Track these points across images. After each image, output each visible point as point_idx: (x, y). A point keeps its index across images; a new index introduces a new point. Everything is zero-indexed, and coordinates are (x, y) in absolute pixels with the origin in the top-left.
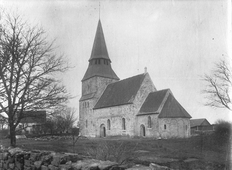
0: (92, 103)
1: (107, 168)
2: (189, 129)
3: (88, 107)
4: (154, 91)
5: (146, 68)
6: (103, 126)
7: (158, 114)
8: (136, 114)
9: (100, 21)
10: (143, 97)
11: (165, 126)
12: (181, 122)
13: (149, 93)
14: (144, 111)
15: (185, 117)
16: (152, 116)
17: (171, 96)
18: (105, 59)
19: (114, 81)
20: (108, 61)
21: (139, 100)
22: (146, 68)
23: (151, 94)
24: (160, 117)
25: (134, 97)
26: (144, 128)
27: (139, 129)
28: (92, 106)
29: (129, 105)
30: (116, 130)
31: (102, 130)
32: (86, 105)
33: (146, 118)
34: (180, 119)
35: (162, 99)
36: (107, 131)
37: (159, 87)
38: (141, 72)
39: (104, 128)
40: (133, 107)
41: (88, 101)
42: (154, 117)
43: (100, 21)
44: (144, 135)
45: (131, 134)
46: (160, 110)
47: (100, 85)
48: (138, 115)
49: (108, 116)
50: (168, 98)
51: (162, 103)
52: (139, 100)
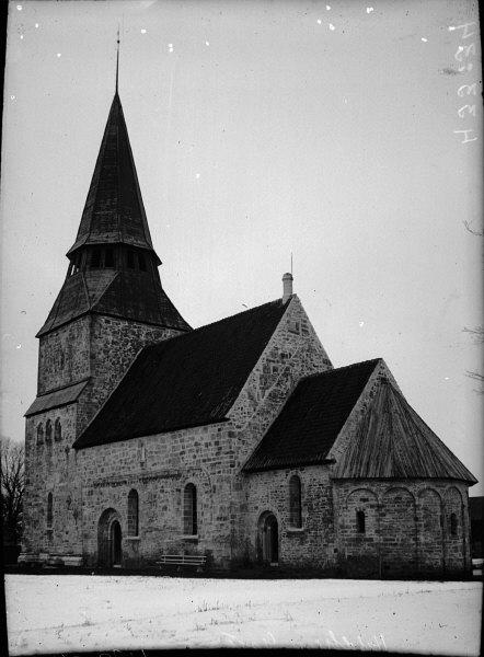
0: (68, 422)
5: (288, 278)
8: (243, 458)
9: (117, 105)
10: (273, 396)
16: (308, 476)
19: (168, 334)
21: (253, 406)
22: (288, 278)
28: (70, 433)
31: (108, 533)
33: (282, 479)
37: (341, 355)
38: (275, 293)
39: (117, 527)
40: (231, 435)
41: (58, 413)
43: (117, 105)
52: (253, 406)
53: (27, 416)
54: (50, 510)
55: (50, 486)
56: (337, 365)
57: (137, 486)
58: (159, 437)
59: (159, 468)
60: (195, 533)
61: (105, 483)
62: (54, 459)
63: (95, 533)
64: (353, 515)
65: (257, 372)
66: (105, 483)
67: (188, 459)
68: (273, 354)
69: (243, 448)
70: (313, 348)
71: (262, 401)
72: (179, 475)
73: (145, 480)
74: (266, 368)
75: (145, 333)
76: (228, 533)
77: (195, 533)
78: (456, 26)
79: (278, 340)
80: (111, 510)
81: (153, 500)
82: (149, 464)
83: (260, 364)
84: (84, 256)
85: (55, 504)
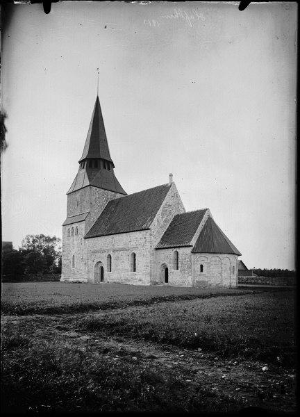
0: (83, 228)
1: (40, 274)
2: (236, 272)
3: (77, 234)
4: (182, 212)
5: (171, 175)
6: (100, 265)
7: (192, 248)
8: (155, 244)
9: (98, 98)
10: (165, 221)
11: (202, 266)
12: (225, 258)
13: (174, 215)
14: (168, 243)
15: (234, 254)
16: (181, 251)
17: (210, 220)
18: (105, 161)
19: (119, 196)
20: (109, 165)
21: (159, 224)
22: (171, 175)
23: (177, 217)
24: (193, 252)
25: (152, 220)
26: (167, 269)
27: (159, 273)
28: (83, 232)
29: (143, 233)
30: (119, 273)
31: (99, 271)
32: (73, 232)
33: (171, 252)
34: (226, 255)
35: (202, 216)
36: (106, 273)
37: (190, 207)
38: (164, 181)
39: (102, 269)
40: (151, 235)
41: (77, 224)
42: (184, 252)
43: (98, 98)
44: (167, 281)
45: (146, 282)
46: (193, 242)
47: (100, 199)
48: (157, 249)
49: (108, 250)
50: (205, 227)
51: (196, 233)
52: (159, 224)
53: (80, 162)
54: (73, 262)
55: (73, 253)
56: (188, 210)
57: (111, 253)
58: (221, 256)
59: (121, 247)
60: (135, 271)
61: (97, 252)
62: (75, 242)
63: (93, 270)
64: (199, 266)
65: (159, 212)
66: (97, 252)
67: (133, 244)
68: (166, 205)
69: (155, 240)
70: (179, 203)
71: (162, 223)
72: (129, 250)
73: (114, 251)
74: (163, 210)
75: (111, 196)
76: (149, 271)
77: (135, 271)
78: (4, 265)
79: (168, 200)
80: (100, 262)
81: (117, 259)
82: (116, 246)
83: (161, 209)
84: (86, 163)
85: (76, 260)
